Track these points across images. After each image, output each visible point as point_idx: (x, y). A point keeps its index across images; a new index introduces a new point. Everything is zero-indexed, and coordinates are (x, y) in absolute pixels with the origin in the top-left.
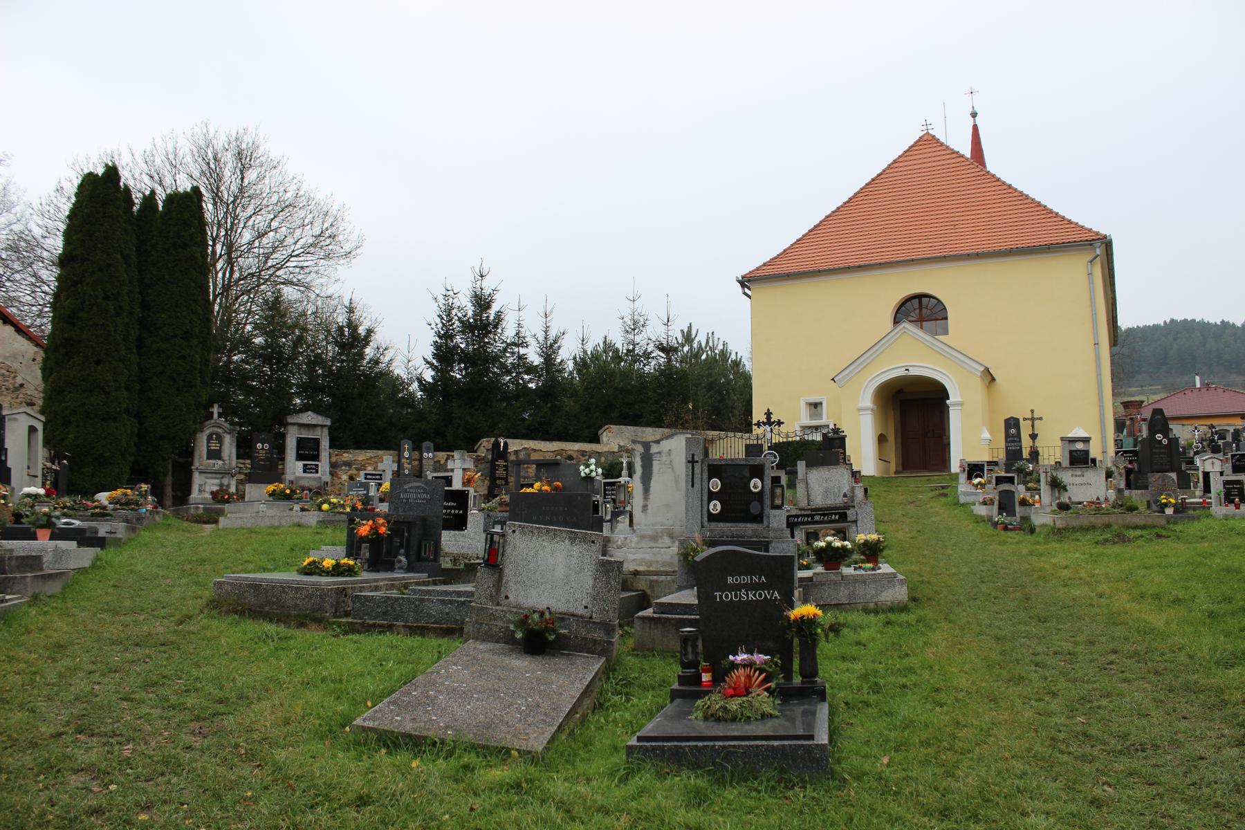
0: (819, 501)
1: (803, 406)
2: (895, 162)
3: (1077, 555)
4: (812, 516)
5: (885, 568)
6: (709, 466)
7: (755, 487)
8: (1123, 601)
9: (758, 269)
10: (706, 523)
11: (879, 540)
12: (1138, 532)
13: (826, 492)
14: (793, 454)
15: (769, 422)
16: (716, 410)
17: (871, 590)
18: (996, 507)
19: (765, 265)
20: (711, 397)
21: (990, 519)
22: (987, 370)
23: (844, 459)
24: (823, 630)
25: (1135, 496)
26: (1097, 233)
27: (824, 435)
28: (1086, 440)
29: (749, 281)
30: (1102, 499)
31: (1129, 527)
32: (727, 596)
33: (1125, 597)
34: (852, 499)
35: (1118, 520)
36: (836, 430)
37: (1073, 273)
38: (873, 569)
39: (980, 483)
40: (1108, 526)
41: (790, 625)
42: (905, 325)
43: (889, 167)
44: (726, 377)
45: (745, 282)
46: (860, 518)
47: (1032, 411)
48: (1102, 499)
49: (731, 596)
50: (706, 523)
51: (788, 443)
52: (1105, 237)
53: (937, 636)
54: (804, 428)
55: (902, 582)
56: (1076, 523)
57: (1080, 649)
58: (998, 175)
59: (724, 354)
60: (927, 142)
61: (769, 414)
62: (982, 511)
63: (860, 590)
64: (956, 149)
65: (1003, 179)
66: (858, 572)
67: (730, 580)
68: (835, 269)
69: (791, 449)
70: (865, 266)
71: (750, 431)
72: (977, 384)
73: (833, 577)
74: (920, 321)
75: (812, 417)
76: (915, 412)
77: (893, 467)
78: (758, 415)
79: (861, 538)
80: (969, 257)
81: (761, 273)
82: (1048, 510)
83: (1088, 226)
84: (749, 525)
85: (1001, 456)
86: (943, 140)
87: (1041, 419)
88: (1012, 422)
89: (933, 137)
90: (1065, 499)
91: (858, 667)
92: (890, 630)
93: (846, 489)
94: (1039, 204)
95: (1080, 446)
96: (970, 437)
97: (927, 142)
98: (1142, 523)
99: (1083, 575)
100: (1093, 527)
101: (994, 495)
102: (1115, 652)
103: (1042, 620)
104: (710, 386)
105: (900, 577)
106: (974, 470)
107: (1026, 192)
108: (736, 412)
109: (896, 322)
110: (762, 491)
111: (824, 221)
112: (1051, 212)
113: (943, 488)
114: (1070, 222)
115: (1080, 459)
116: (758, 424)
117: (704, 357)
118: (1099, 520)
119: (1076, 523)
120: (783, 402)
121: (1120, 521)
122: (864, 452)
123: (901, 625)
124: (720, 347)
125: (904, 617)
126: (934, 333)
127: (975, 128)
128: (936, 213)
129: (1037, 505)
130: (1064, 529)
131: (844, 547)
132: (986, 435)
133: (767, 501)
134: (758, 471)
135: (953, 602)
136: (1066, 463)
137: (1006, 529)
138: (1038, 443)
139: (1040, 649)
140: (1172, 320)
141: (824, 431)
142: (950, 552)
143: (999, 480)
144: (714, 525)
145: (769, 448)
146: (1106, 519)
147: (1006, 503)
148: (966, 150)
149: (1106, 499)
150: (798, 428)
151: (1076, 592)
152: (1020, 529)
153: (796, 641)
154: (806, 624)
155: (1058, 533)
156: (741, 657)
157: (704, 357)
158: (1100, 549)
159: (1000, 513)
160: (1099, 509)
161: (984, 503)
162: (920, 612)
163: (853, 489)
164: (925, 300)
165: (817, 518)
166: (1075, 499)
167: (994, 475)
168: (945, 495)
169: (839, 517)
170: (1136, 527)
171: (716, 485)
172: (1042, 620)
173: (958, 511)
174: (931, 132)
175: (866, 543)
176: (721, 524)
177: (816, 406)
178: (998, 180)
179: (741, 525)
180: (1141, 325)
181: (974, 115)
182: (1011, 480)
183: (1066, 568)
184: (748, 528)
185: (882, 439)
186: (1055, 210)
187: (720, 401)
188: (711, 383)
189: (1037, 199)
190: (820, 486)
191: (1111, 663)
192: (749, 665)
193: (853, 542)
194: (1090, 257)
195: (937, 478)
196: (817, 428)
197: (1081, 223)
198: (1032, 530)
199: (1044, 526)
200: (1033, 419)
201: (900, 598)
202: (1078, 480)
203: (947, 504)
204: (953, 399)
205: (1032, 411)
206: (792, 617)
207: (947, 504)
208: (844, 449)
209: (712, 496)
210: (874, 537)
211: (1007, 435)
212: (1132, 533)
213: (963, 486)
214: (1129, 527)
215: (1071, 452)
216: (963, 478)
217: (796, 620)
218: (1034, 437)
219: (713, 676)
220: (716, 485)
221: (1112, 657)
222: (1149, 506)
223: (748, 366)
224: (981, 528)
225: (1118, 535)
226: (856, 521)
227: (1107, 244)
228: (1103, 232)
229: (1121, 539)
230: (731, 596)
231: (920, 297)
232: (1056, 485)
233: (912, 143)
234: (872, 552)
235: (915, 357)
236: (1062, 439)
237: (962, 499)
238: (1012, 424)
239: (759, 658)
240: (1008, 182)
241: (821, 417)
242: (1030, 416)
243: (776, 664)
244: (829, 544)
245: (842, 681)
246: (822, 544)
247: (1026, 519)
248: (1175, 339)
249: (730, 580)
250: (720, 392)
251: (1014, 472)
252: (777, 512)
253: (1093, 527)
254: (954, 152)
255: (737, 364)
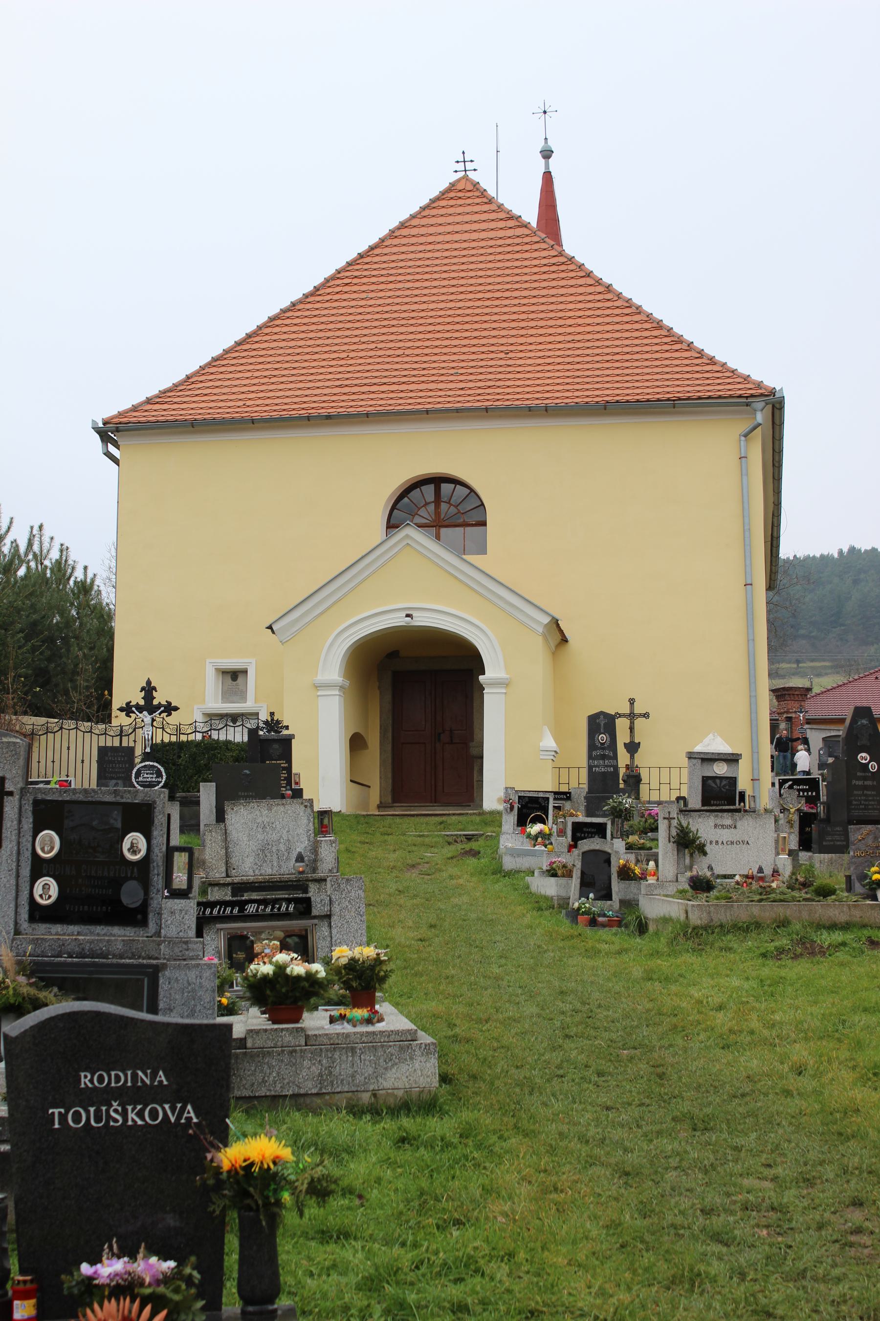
0: (248, 868)
1: (210, 675)
2: (403, 225)
3: (736, 982)
4: (242, 905)
5: (392, 1018)
6: (36, 803)
7: (133, 849)
8: (845, 1088)
9: (135, 409)
10: (25, 925)
11: (378, 961)
12: (838, 937)
13: (264, 851)
14: (189, 764)
15: (149, 706)
16: (42, 677)
17: (365, 1065)
18: (575, 881)
19: (149, 401)
20: (34, 649)
21: (564, 903)
22: (556, 622)
23: (289, 779)
24: (294, 1191)
25: (823, 865)
26: (759, 385)
27: (253, 733)
28: (732, 759)
29: (117, 430)
30: (768, 871)
31: (820, 926)
32: (77, 1117)
33: (848, 1076)
34: (314, 865)
35: (803, 911)
36: (273, 725)
37: (714, 450)
38: (369, 1021)
39: (540, 833)
40: (783, 923)
41: (220, 1184)
42: (410, 533)
43: (392, 234)
44: (63, 612)
45: (110, 432)
46: (336, 909)
47: (632, 702)
48: (768, 871)
49: (88, 1116)
50: (25, 925)
51: (181, 745)
52: (773, 392)
53: (506, 1175)
54: (211, 717)
55: (427, 1049)
56: (724, 917)
57: (789, 1196)
58: (589, 266)
59: (61, 568)
60: (464, 194)
61: (149, 690)
62: (549, 887)
63: (343, 1067)
64: (516, 212)
65: (598, 273)
66: (338, 1028)
67: (85, 1080)
68: (281, 419)
69: (185, 757)
70: (339, 416)
71: (106, 718)
72: (536, 647)
73: (288, 1038)
74: (436, 525)
75: (227, 695)
76: (421, 693)
77: (375, 796)
78: (125, 689)
79: (342, 953)
80: (530, 412)
81: (140, 417)
82: (672, 889)
83: (743, 370)
84: (116, 930)
85: (578, 781)
86: (492, 192)
87: (646, 715)
88: (602, 721)
89: (476, 185)
90: (701, 869)
91: (352, 1254)
92: (406, 1155)
93: (302, 845)
94: (659, 325)
95: (720, 769)
96: (521, 745)
97: (464, 194)
98: (843, 918)
99: (755, 1024)
100: (752, 927)
101: (574, 860)
102: (857, 1203)
103: (700, 1125)
104: (33, 630)
105: (425, 1038)
106: (530, 808)
107: (637, 301)
108: (81, 682)
109: (392, 525)
110: (147, 859)
111: (265, 325)
112: (680, 340)
113: (469, 838)
114: (712, 361)
115: (721, 796)
116: (127, 709)
117: (22, 572)
118: (767, 912)
119: (724, 917)
120: (173, 664)
121: (805, 915)
122: (324, 768)
123: (430, 1145)
124: (55, 555)
125: (436, 1126)
126: (462, 551)
127: (548, 178)
128: (469, 328)
129: (651, 880)
130: (705, 928)
131: (310, 977)
132: (549, 742)
133: (158, 881)
134: (140, 817)
135: (520, 1085)
136: (695, 802)
137: (593, 923)
138: (640, 759)
139: (714, 1198)
140: (852, 550)
141: (251, 724)
142: (496, 970)
143: (580, 831)
144: (42, 928)
145: (146, 757)
146: (781, 911)
147: (596, 877)
148: (529, 212)
149: (776, 872)
150: (199, 718)
151: (752, 1062)
152: (619, 924)
153: (233, 1216)
154: (257, 1181)
155: (694, 935)
156: (110, 1268)
157: (22, 572)
158: (769, 970)
159: (583, 894)
160: (766, 891)
161: (552, 873)
162: (466, 1115)
163: (315, 848)
164: (446, 488)
165: (251, 909)
166: (718, 871)
167: (570, 821)
168: (475, 854)
169: (290, 904)
170: (833, 927)
171: (49, 844)
172: (700, 1125)
173: (500, 885)
174: (471, 175)
175: (353, 965)
176: (58, 928)
177: (235, 675)
178: (589, 274)
179: (99, 929)
180: (800, 555)
181: (547, 154)
182: (600, 830)
183: (720, 1008)
184: (116, 937)
185: (356, 743)
186: (688, 337)
187: (49, 660)
188: (35, 624)
189: (657, 315)
190: (253, 840)
191: (858, 1231)
192: (125, 1288)
193: (327, 962)
194: (745, 427)
195: (458, 820)
196: (234, 718)
197: (732, 365)
198: (642, 928)
199: (666, 920)
200: (632, 716)
201: (423, 1082)
202: (725, 835)
203: (481, 872)
204: (492, 673)
205: (632, 702)
206: (226, 1165)
207: (481, 872)
208: (289, 761)
209: (39, 868)
210: (369, 952)
211: (592, 746)
212: (826, 938)
213: (510, 839)
214: (820, 926)
215: (705, 779)
216: (509, 821)
217: (233, 1171)
218: (633, 748)
219: (39, 1307)
220: (49, 844)
221: (856, 1216)
222: (849, 888)
223: (107, 596)
224: (547, 922)
225: (802, 941)
226: (328, 917)
227: (775, 405)
228: (770, 382)
229: (807, 949)
230: (88, 1116)
231: (437, 481)
232: (686, 843)
233: (435, 193)
234: (361, 984)
235: (424, 591)
236: (691, 756)
237: (509, 863)
238: (601, 725)
239: (153, 1267)
240: (607, 280)
241: (244, 698)
242: (627, 711)
243: (189, 1280)
244: (281, 969)
245: (324, 1296)
246: (267, 969)
247: (629, 905)
248: (856, 582)
249: (85, 1080)
250: (51, 640)
251: (604, 815)
252: (178, 904)
253: (757, 925)
254: (511, 217)
255: (85, 588)
